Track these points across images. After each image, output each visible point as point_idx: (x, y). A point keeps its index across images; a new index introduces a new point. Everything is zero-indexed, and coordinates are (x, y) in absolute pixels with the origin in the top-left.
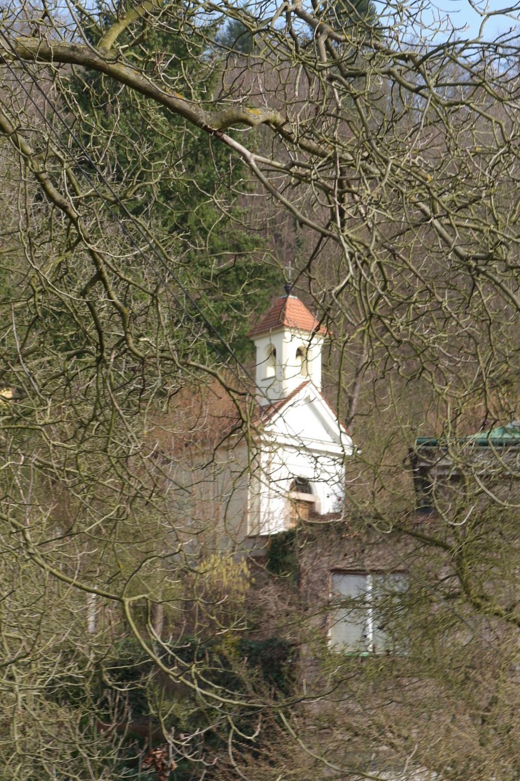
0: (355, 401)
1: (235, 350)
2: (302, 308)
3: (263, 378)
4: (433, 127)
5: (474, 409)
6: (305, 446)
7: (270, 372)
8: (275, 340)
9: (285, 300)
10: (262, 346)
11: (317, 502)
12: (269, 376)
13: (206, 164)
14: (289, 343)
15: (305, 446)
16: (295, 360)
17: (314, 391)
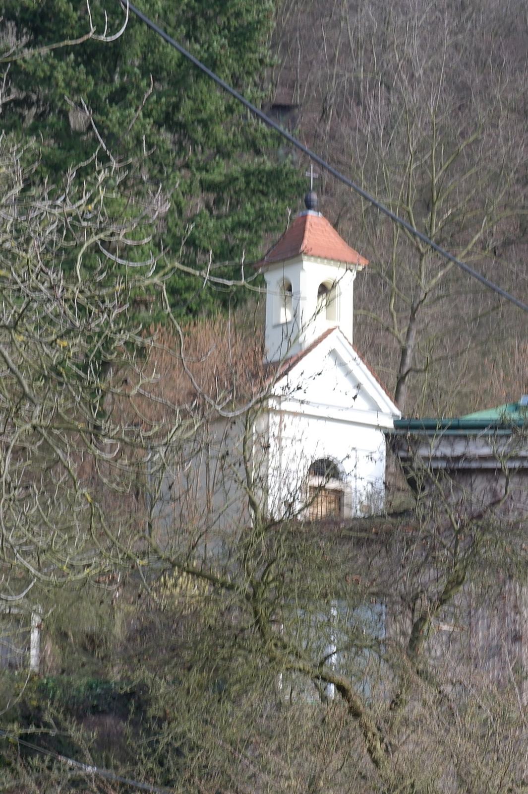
0: (409, 352)
1: (238, 300)
2: (329, 228)
3: (274, 322)
4: (7, 332)
5: (405, 14)
6: (329, 419)
7: (285, 315)
8: (288, 272)
9: (305, 218)
10: (273, 279)
11: (347, 490)
12: (283, 320)
13: (208, 31)
14: (311, 274)
15: (329, 419)
16: (319, 293)
17: (342, 340)
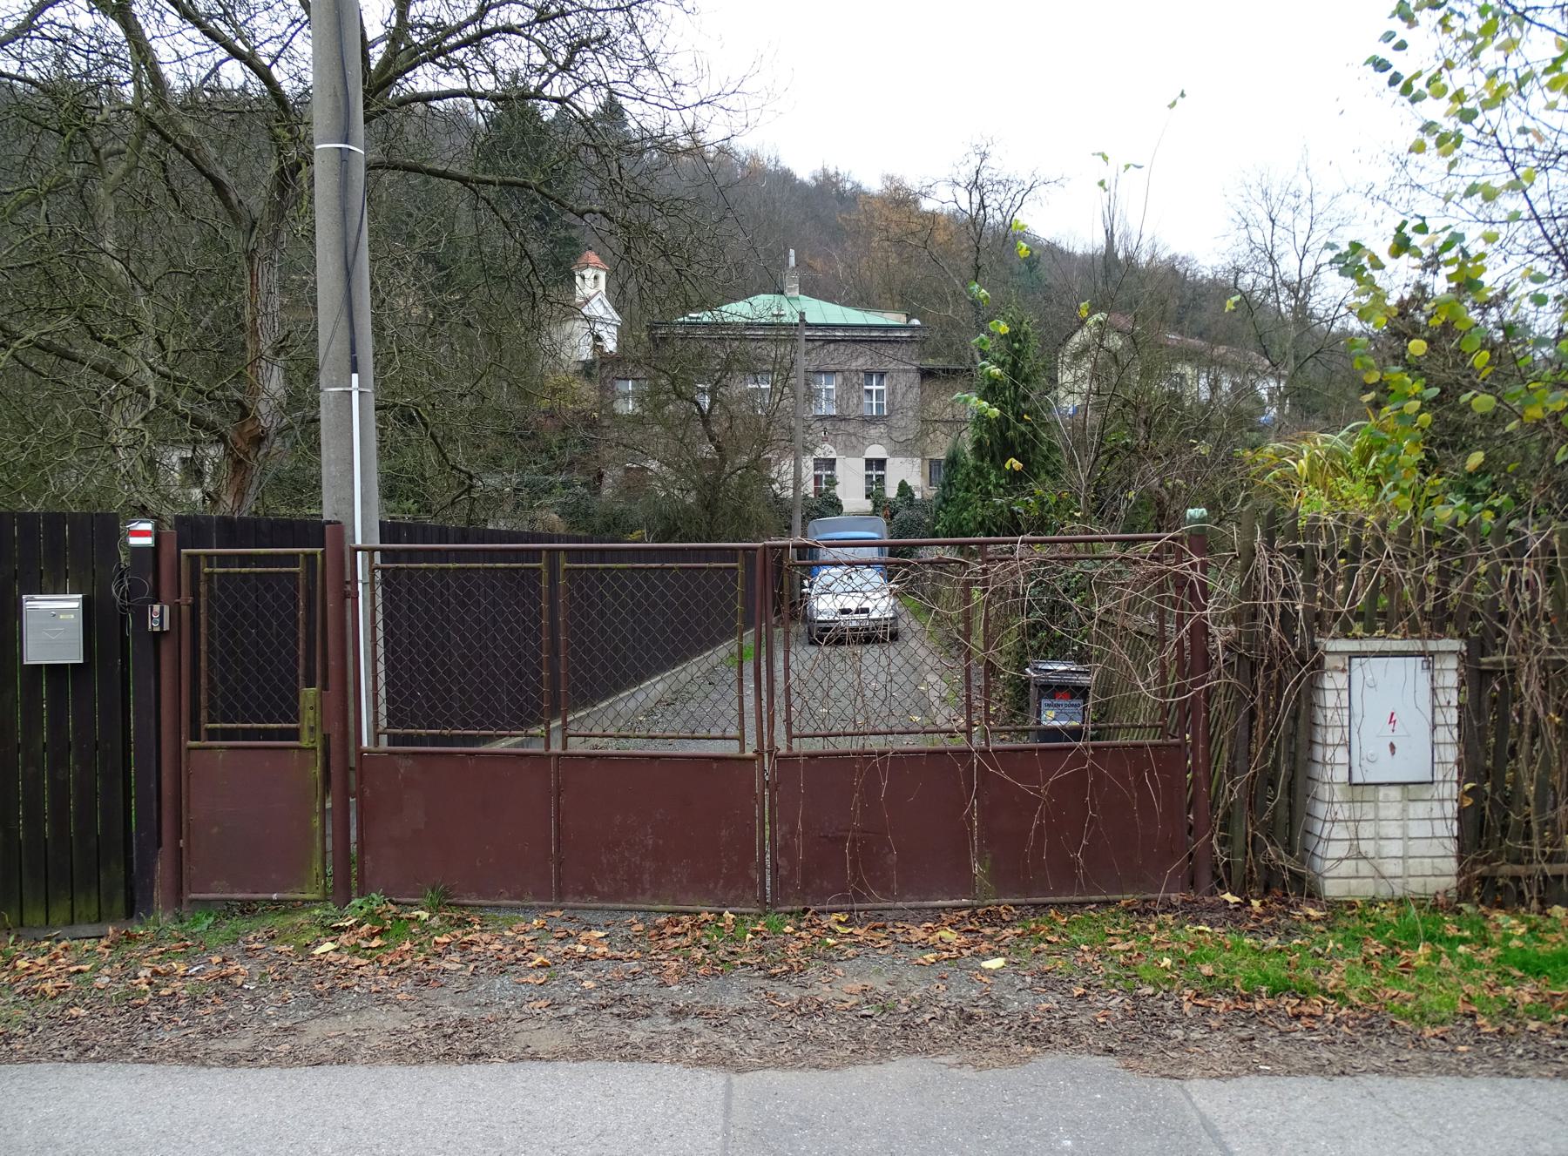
17: (602, 296)
